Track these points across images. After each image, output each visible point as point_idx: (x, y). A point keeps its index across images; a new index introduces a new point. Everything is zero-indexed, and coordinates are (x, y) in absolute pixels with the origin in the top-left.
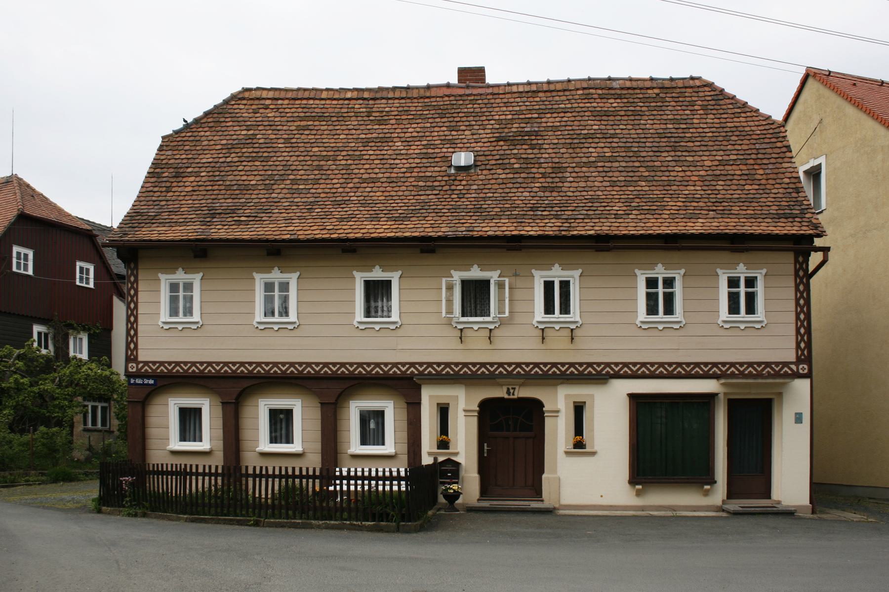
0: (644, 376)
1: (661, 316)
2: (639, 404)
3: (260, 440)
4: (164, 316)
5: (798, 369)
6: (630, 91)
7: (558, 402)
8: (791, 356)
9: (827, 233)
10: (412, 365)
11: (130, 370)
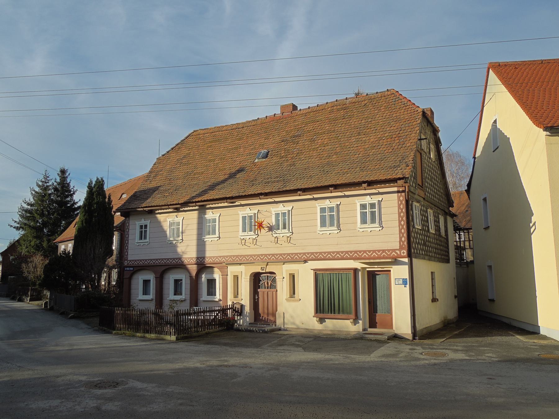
0: (329, 259)
2: (317, 274)
3: (170, 295)
4: (137, 239)
5: (400, 253)
7: (282, 272)
9: (66, 169)
11: (405, 254)
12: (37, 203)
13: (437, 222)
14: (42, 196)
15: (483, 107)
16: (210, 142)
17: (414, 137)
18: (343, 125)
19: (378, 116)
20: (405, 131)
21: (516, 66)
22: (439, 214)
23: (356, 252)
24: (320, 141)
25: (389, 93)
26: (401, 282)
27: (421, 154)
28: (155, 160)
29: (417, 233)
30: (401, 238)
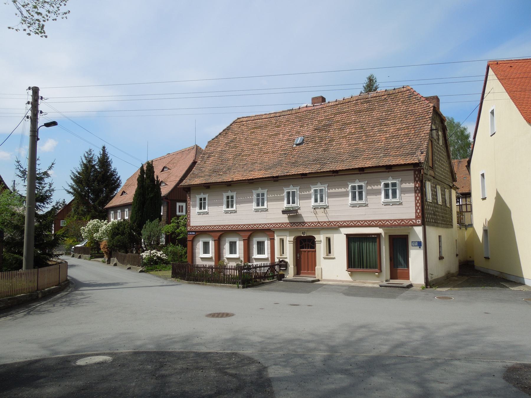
1: (391, 199)
2: (350, 238)
3: (226, 254)
6: (375, 98)
7: (320, 238)
8: (414, 216)
10: (271, 224)
12: (83, 172)
13: (443, 195)
14: (88, 167)
15: (483, 98)
16: (253, 128)
17: (427, 128)
18: (367, 117)
19: (396, 109)
20: (419, 123)
21: (511, 64)
22: (445, 188)
23: (380, 221)
24: (348, 130)
25: (405, 89)
26: (416, 244)
27: (432, 141)
28: (207, 144)
29: (429, 205)
30: (416, 210)
